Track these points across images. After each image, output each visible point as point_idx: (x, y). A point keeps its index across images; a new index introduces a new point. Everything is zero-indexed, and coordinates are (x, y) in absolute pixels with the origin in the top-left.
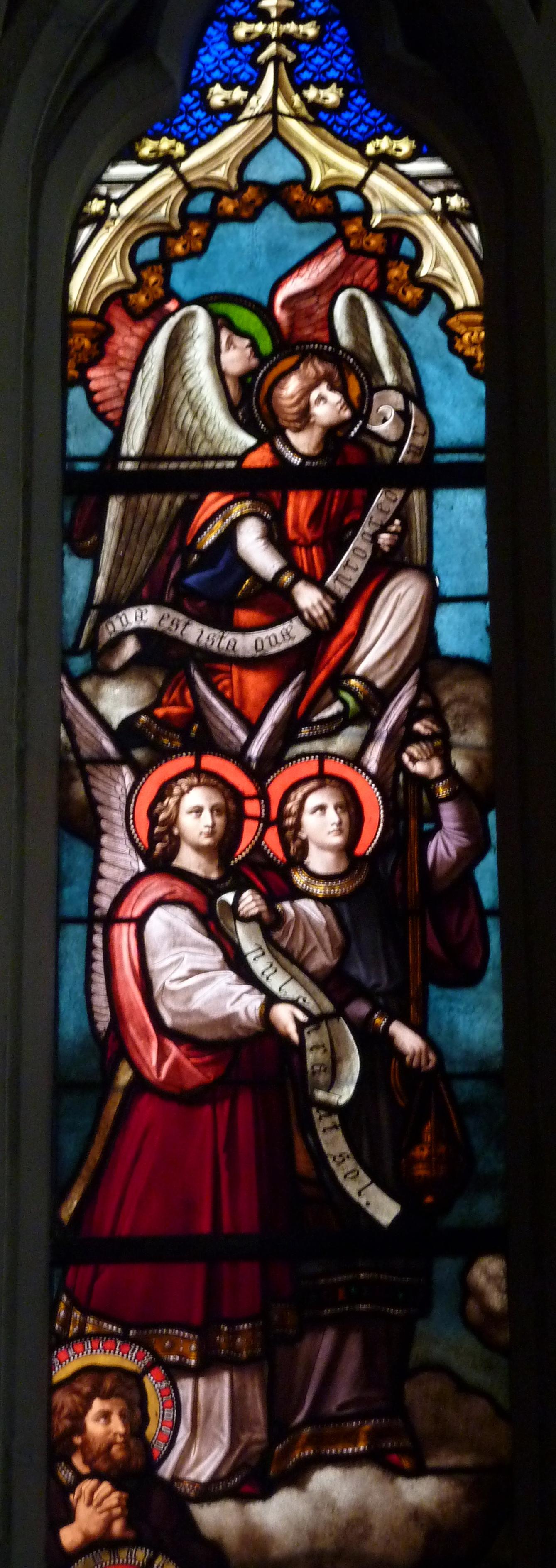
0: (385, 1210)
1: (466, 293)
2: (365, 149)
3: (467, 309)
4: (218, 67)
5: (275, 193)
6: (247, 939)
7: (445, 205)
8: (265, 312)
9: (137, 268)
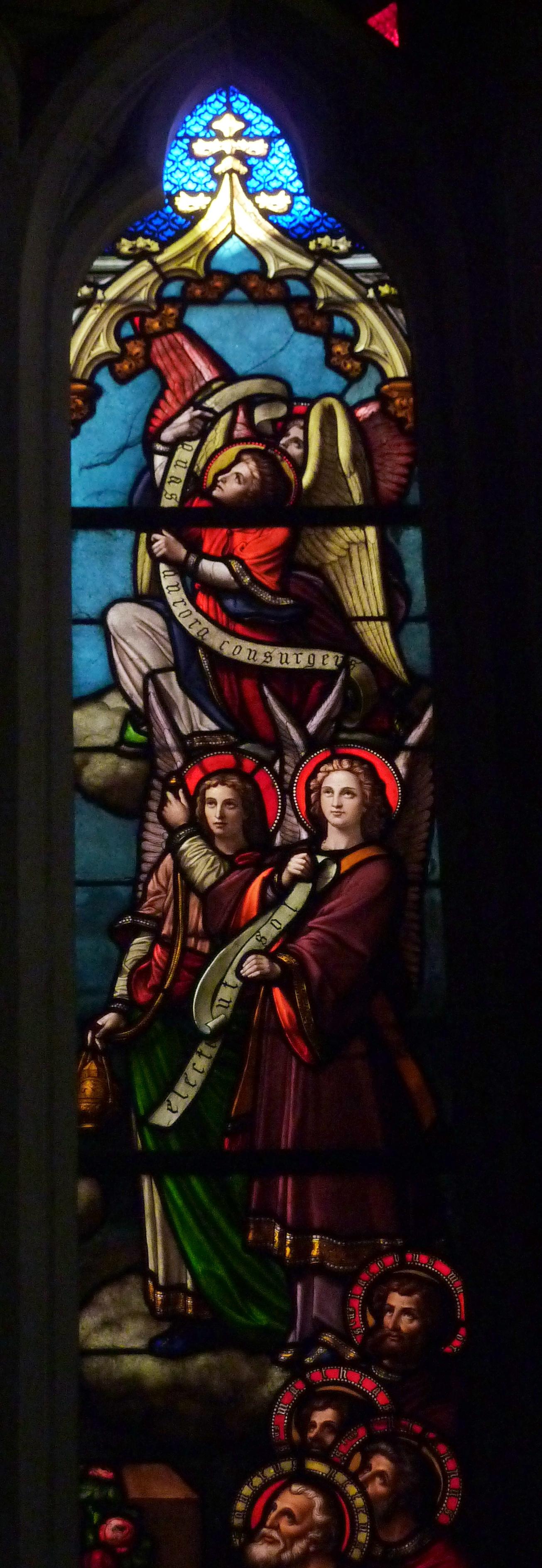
1: (396, 366)
2: (308, 245)
3: (397, 379)
4: (322, 224)
7: (377, 292)
9: (121, 341)
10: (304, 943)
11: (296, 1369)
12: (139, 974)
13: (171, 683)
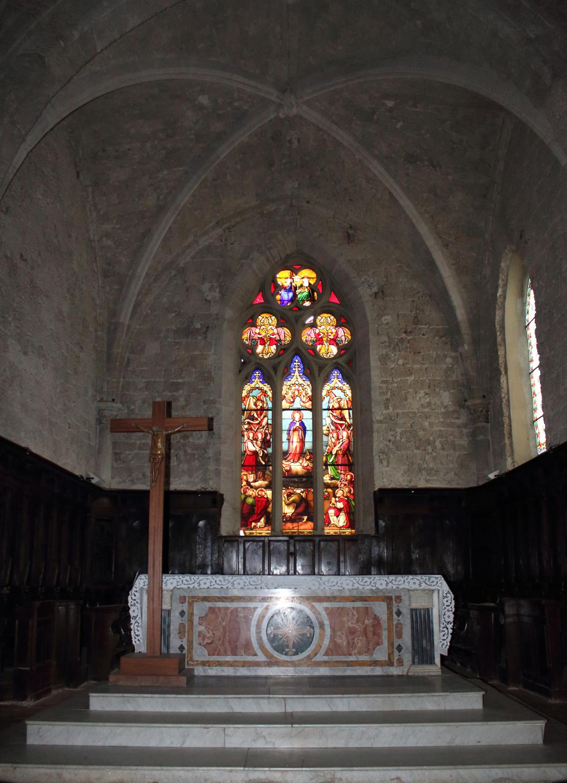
0: (264, 463)
1: (271, 396)
5: (257, 388)
6: (255, 444)
8: (256, 397)
10: (341, 447)
11: (340, 481)
12: (328, 450)
13: (331, 424)
